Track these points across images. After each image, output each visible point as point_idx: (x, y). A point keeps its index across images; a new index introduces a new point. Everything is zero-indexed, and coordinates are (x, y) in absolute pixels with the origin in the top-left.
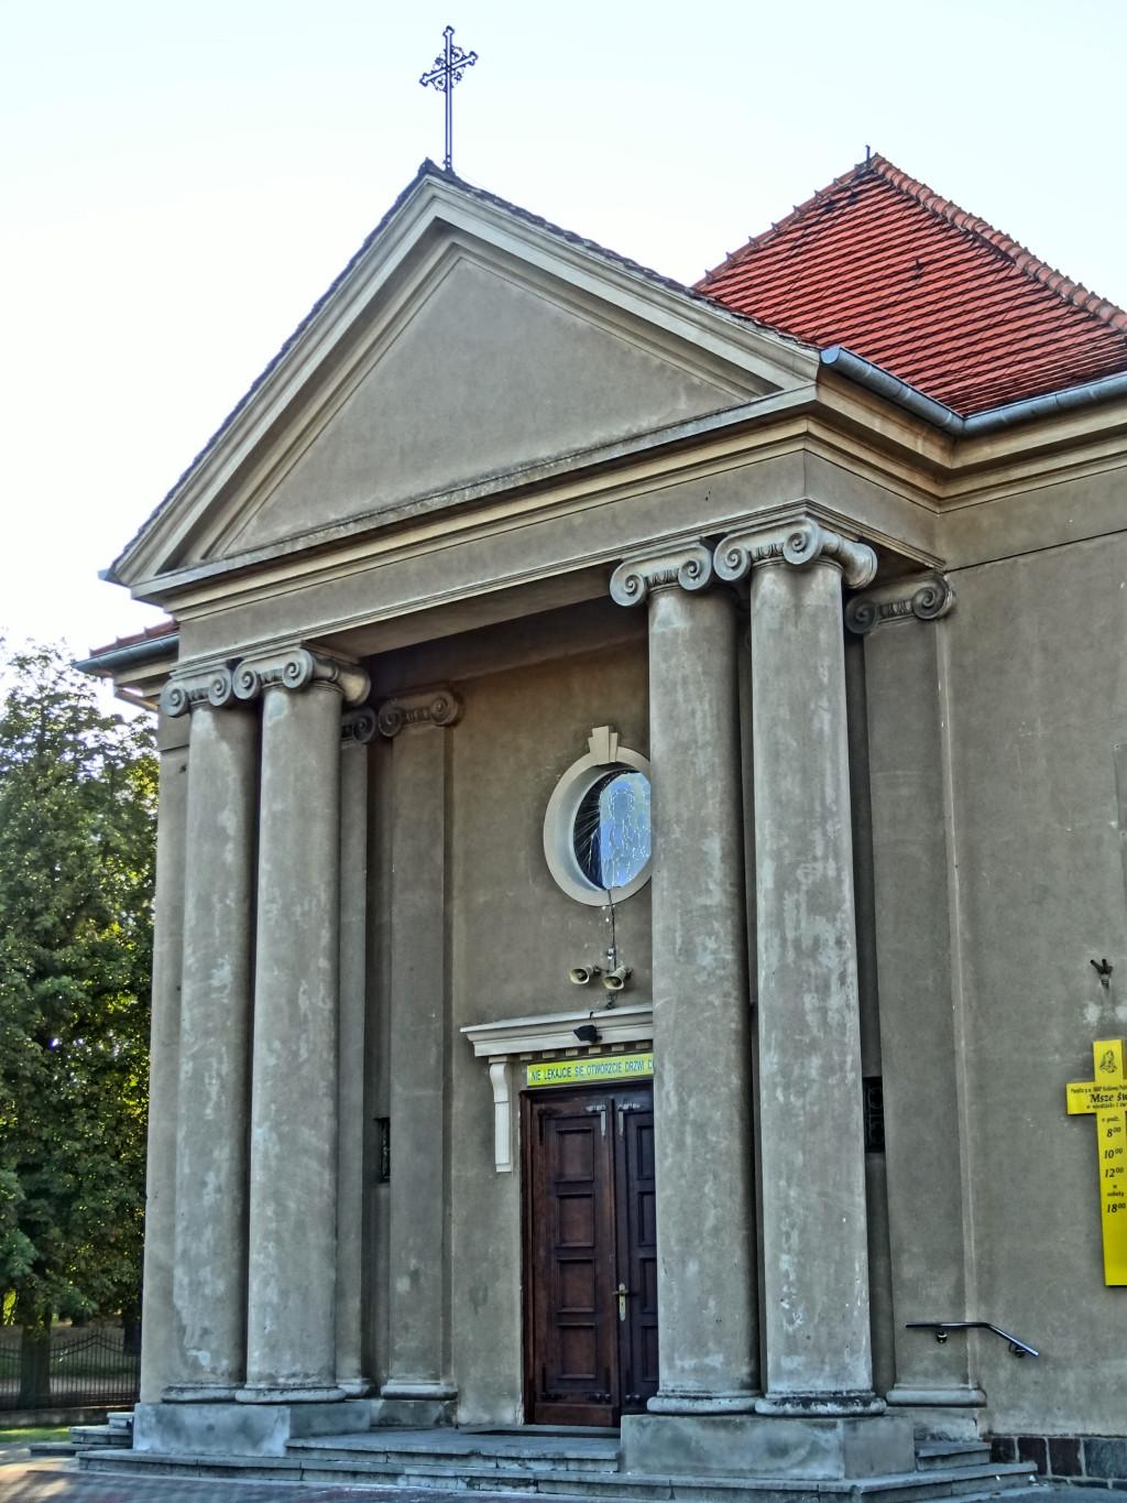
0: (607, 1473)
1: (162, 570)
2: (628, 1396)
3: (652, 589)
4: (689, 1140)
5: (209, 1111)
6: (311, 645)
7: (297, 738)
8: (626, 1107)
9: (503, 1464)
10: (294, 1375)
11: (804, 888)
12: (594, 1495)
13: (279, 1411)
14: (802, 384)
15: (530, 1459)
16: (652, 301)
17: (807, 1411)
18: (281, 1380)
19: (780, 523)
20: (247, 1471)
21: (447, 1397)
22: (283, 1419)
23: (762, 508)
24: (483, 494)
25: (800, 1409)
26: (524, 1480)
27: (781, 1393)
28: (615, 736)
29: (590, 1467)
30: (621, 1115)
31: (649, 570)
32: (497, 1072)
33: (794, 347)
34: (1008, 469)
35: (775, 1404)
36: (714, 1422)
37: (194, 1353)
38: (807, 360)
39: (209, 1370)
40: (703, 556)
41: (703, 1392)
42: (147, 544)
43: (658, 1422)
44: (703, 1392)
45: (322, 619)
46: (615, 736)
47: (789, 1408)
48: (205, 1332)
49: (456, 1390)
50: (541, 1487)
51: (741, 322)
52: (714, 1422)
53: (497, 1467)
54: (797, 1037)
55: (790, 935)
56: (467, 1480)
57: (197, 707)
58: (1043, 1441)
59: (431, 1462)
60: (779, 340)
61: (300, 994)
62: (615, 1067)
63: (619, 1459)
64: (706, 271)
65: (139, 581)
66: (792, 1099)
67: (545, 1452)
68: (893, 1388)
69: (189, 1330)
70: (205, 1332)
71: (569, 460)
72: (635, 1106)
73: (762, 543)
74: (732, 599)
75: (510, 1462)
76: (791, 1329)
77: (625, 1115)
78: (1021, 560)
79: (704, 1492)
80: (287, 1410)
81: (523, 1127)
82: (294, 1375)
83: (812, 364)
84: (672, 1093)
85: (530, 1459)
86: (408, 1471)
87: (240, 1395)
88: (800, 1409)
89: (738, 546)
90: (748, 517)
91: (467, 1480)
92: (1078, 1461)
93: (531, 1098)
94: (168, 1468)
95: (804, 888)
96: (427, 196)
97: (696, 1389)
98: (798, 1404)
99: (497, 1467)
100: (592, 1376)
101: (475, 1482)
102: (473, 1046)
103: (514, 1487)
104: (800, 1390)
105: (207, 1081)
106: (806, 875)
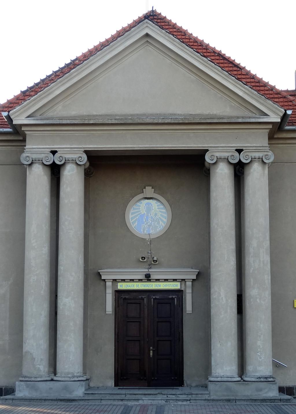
0: (206, 397)
1: (28, 117)
2: (153, 378)
3: (219, 160)
4: (229, 311)
5: (42, 292)
6: (86, 152)
7: (72, 180)
8: (154, 297)
9: (168, 396)
10: (78, 373)
11: (265, 248)
12: (210, 403)
13: (80, 383)
14: (276, 116)
15: (179, 394)
16: (228, 81)
17: (267, 380)
18: (75, 374)
19: (262, 150)
20: (125, 400)
21: (87, 380)
22: (82, 386)
23: (255, 145)
24: (166, 122)
25: (265, 380)
26: (186, 400)
27: (258, 376)
28: (153, 190)
29: (200, 396)
30: (152, 299)
31: (218, 154)
32: (109, 284)
33: (277, 107)
34: (286, 140)
35: (258, 378)
36: (239, 383)
37: (38, 366)
38: (281, 111)
39: (43, 371)
40: (237, 154)
41: (232, 376)
42: (23, 108)
43: (221, 384)
44: (232, 376)
45: (91, 145)
46: (153, 190)
47: (262, 380)
48: (41, 359)
49: (89, 377)
50: (191, 401)
51: (260, 95)
52: (239, 383)
53: (167, 397)
54: (263, 286)
55: (262, 260)
56: (165, 400)
57: (35, 163)
58: (284, 387)
59: (130, 395)
60: (272, 103)
61: (80, 259)
62: (151, 286)
63: (209, 394)
64: (106, 39)
65: (17, 118)
66: (262, 302)
67: (185, 392)
68: (243, 375)
69: (36, 359)
70: (41, 359)
71: (198, 119)
72: (157, 297)
73: (257, 155)
74: (239, 170)
75: (172, 395)
76: (260, 360)
77: (153, 299)
78: (286, 164)
79: (246, 401)
80: (84, 383)
81: (115, 300)
82: (78, 373)
83: (282, 112)
84: (224, 298)
85: (179, 394)
86: (143, 398)
87: (55, 378)
88: (265, 380)
89: (248, 154)
90: (251, 147)
91: (165, 400)
92: (294, 392)
93: (118, 293)
94: (43, 401)
95: (265, 248)
96: (145, 25)
97: (230, 375)
98: (264, 379)
99: (167, 397)
100: (138, 373)
101: (168, 401)
102: (101, 276)
103: (182, 402)
104: (263, 375)
105: (42, 283)
106: (265, 244)
